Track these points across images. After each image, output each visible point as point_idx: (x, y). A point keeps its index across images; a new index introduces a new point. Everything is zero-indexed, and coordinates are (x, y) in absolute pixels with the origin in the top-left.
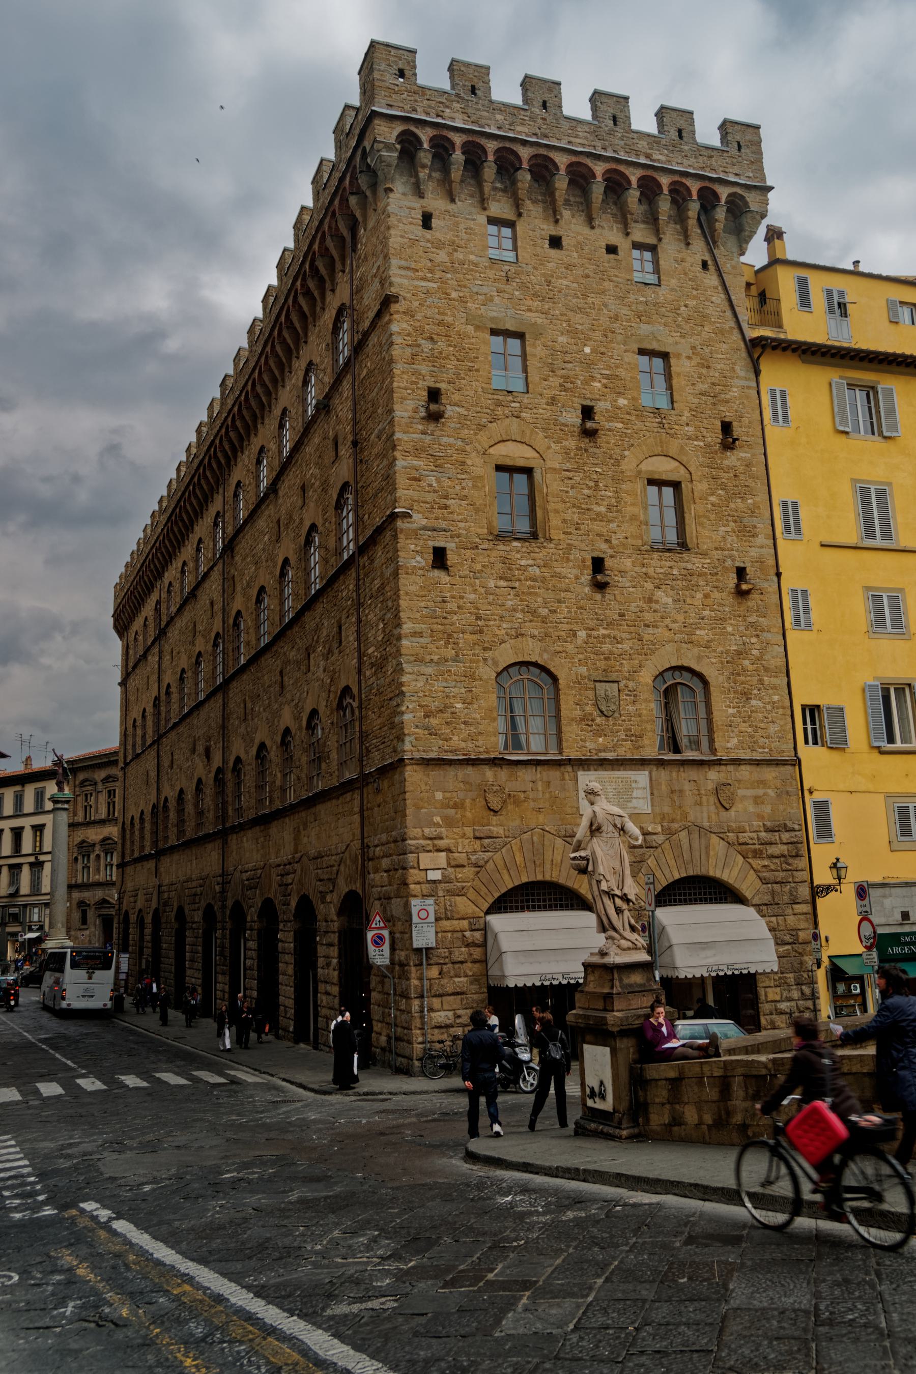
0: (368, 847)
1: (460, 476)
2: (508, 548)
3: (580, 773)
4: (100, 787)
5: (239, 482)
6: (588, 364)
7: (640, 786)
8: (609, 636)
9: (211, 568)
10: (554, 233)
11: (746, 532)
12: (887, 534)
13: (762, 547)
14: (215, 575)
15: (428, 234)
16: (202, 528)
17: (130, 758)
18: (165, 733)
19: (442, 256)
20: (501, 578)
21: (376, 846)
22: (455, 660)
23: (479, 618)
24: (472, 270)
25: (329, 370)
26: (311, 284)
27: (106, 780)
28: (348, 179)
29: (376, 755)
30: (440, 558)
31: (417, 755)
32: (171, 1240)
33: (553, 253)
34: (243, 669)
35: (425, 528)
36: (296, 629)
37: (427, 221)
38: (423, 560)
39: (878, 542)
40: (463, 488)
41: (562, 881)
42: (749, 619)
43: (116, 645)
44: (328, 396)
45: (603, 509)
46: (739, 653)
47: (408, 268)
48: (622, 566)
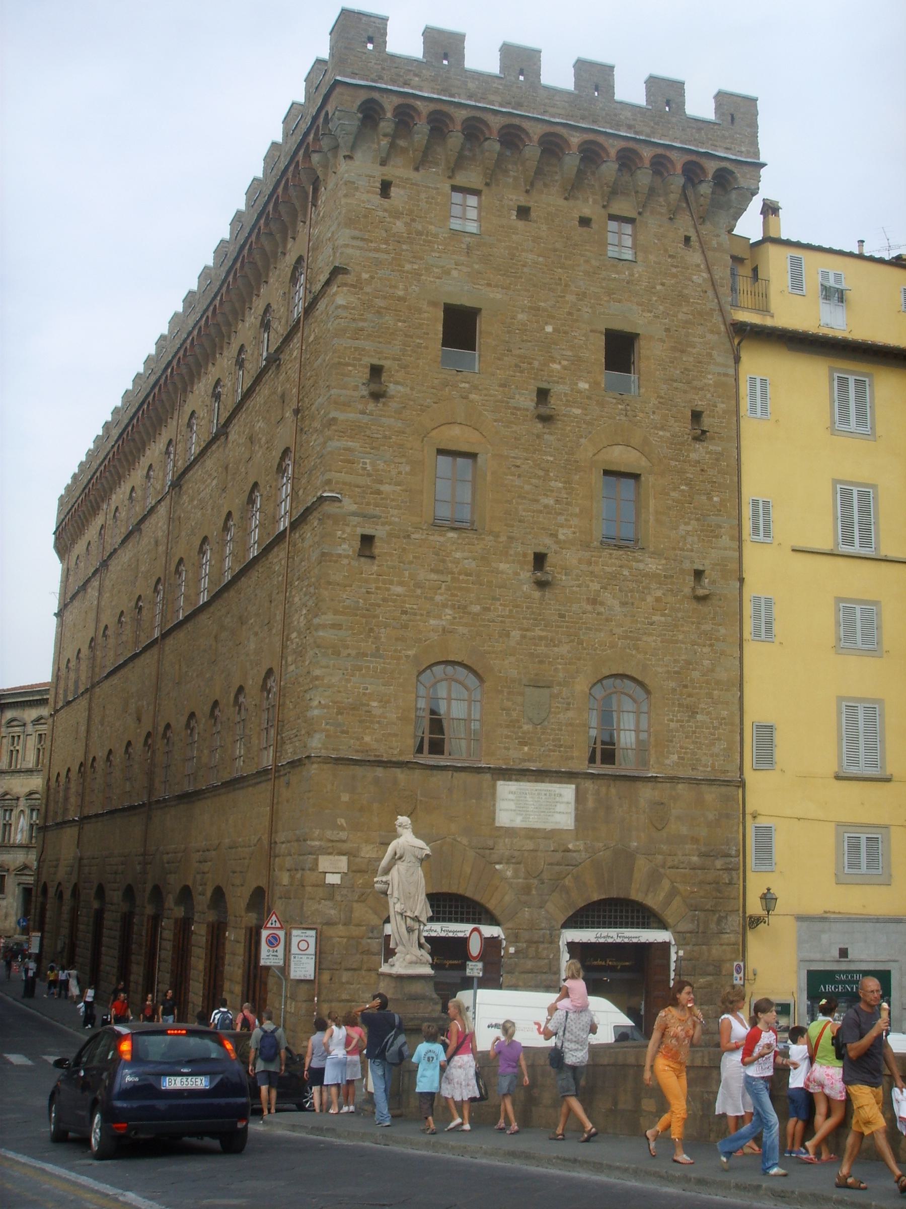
0: (276, 842)
1: (397, 460)
2: (442, 539)
3: (500, 783)
4: (30, 729)
5: (193, 412)
7: (565, 800)
8: (545, 638)
9: (159, 502)
10: (523, 204)
12: (866, 541)
13: (725, 549)
14: (162, 510)
15: (386, 203)
16: (154, 451)
17: (60, 704)
18: (98, 683)
19: (399, 226)
20: (432, 571)
21: (283, 843)
22: (376, 654)
23: (405, 612)
24: (430, 242)
25: (283, 321)
26: (273, 226)
27: (38, 721)
28: (312, 135)
29: (289, 748)
31: (324, 753)
33: (520, 224)
34: (180, 625)
35: (354, 514)
36: (232, 593)
37: (385, 188)
38: (348, 548)
39: (856, 549)
40: (400, 473)
41: (468, 894)
42: (703, 627)
43: (54, 567)
44: (279, 350)
45: (551, 502)
46: (688, 663)
47: (362, 239)
48: (566, 560)
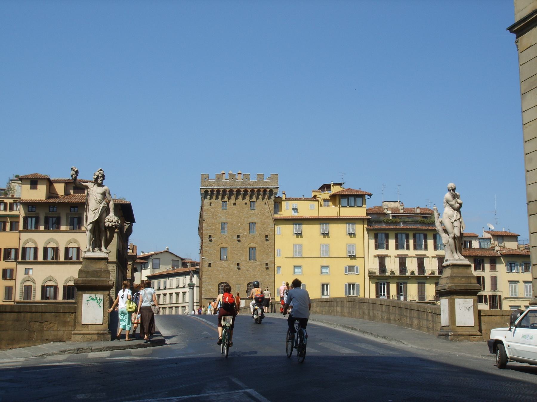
6: (239, 227)
11: (269, 256)
19: (213, 210)
30: (210, 265)
32: (94, 277)
